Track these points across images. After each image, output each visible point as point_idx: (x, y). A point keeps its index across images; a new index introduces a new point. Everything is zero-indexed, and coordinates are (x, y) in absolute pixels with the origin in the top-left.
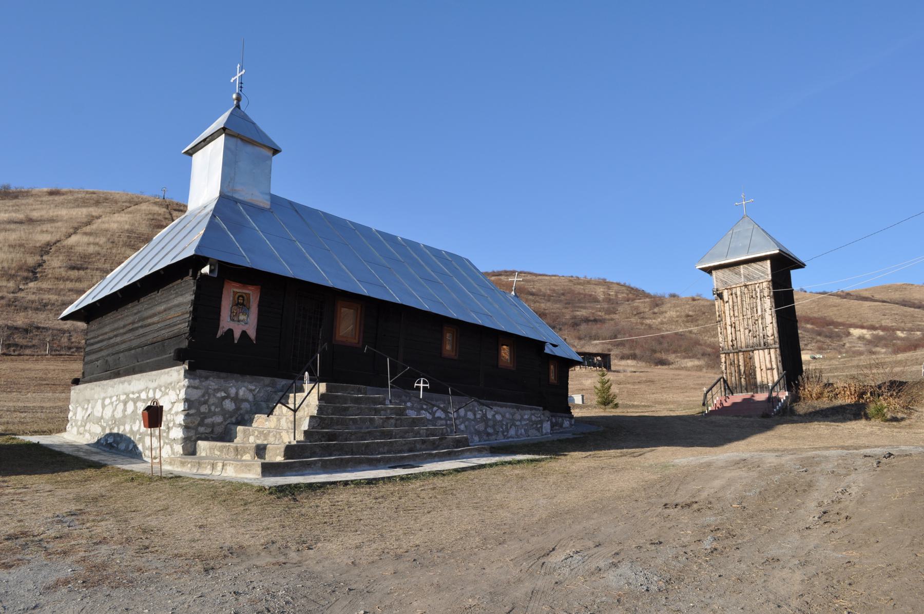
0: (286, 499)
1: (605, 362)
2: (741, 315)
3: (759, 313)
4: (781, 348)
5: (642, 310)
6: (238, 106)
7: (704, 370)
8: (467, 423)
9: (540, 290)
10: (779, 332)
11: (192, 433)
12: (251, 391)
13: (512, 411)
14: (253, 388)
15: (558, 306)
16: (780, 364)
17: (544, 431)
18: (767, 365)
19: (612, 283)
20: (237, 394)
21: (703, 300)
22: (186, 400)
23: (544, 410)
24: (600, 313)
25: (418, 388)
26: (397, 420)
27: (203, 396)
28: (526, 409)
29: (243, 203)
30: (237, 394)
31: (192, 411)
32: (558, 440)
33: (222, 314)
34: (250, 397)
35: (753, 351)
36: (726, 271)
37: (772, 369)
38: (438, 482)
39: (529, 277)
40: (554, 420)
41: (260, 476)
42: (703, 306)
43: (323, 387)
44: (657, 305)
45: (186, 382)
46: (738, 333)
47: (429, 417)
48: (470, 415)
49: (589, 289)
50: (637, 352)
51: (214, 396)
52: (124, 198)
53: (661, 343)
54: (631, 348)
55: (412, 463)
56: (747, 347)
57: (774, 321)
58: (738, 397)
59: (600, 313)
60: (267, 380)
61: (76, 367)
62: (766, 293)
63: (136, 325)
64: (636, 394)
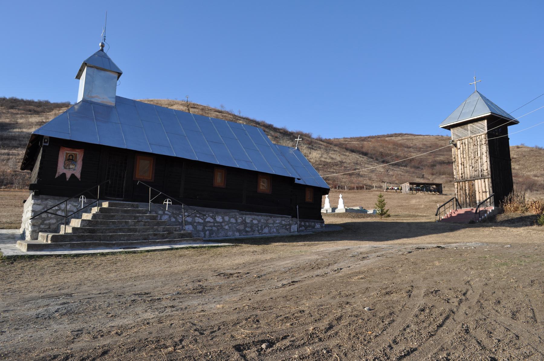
2: (467, 157)
3: (479, 155)
4: (492, 177)
6: (102, 50)
8: (230, 225)
10: (491, 167)
11: (36, 228)
12: (75, 206)
13: (265, 218)
14: (77, 204)
16: (491, 189)
17: (292, 230)
18: (483, 189)
21: (525, 147)
22: (33, 211)
23: (292, 217)
25: (166, 204)
26: (146, 222)
33: (59, 165)
35: (474, 180)
36: (459, 128)
37: (486, 192)
39: (410, 137)
42: (525, 151)
46: (465, 169)
48: (233, 220)
52: (166, 103)
56: (471, 177)
57: (488, 160)
58: (462, 211)
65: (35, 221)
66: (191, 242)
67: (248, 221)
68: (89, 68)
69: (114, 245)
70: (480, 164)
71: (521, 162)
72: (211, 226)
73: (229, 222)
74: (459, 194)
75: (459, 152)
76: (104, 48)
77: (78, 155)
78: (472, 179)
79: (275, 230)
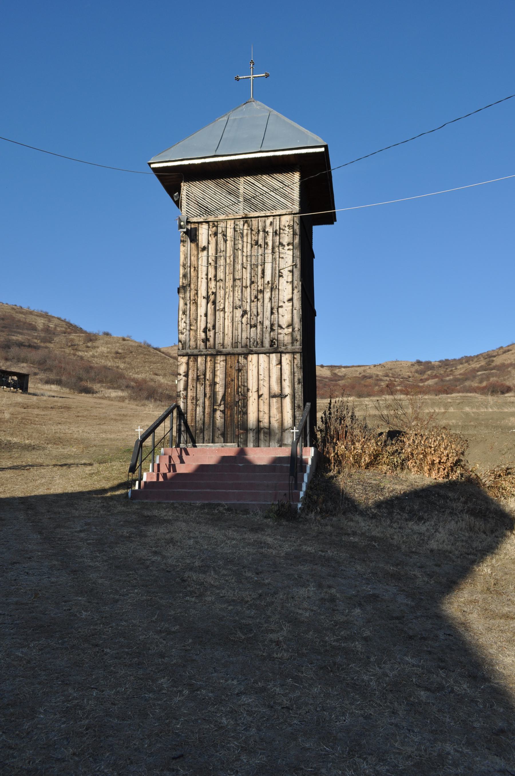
2: (229, 278)
3: (268, 277)
5: (76, 342)
7: (127, 401)
16: (299, 388)
19: (54, 317)
21: (132, 341)
24: (36, 341)
35: (245, 356)
37: (281, 396)
42: (132, 346)
44: (91, 340)
46: (220, 315)
49: (30, 319)
50: (64, 378)
53: (88, 372)
54: (57, 374)
56: (235, 344)
58: (209, 453)
59: (36, 341)
62: (286, 238)
70: (267, 305)
71: (127, 360)
74: (190, 394)
75: (203, 261)
78: (239, 350)
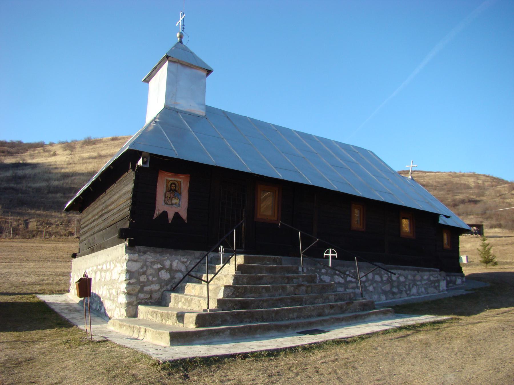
0: (177, 376)
1: (479, 230)
5: (503, 192)
6: (181, 42)
8: (375, 285)
9: (429, 182)
12: (183, 263)
13: (413, 273)
14: (185, 260)
15: (442, 193)
17: (441, 289)
19: (480, 175)
20: (171, 265)
22: (128, 272)
24: (472, 197)
25: (327, 257)
26: (308, 287)
27: (142, 268)
28: (426, 271)
29: (183, 113)
30: (171, 265)
31: (132, 281)
32: (454, 297)
34: (183, 268)
38: (342, 352)
39: (420, 174)
40: (448, 279)
41: (169, 345)
43: (240, 259)
45: (127, 257)
47: (342, 281)
48: (377, 278)
49: (463, 180)
50: (502, 222)
51: (151, 267)
54: (497, 220)
55: (320, 328)
60: (198, 253)
61: (74, 246)
63: (103, 212)
64: (507, 253)
65: (131, 288)
66: (381, 316)
67: (394, 278)
68: (171, 63)
69: (287, 327)
72: (353, 288)
73: (373, 281)
76: (183, 40)
77: (182, 184)
79: (423, 289)
